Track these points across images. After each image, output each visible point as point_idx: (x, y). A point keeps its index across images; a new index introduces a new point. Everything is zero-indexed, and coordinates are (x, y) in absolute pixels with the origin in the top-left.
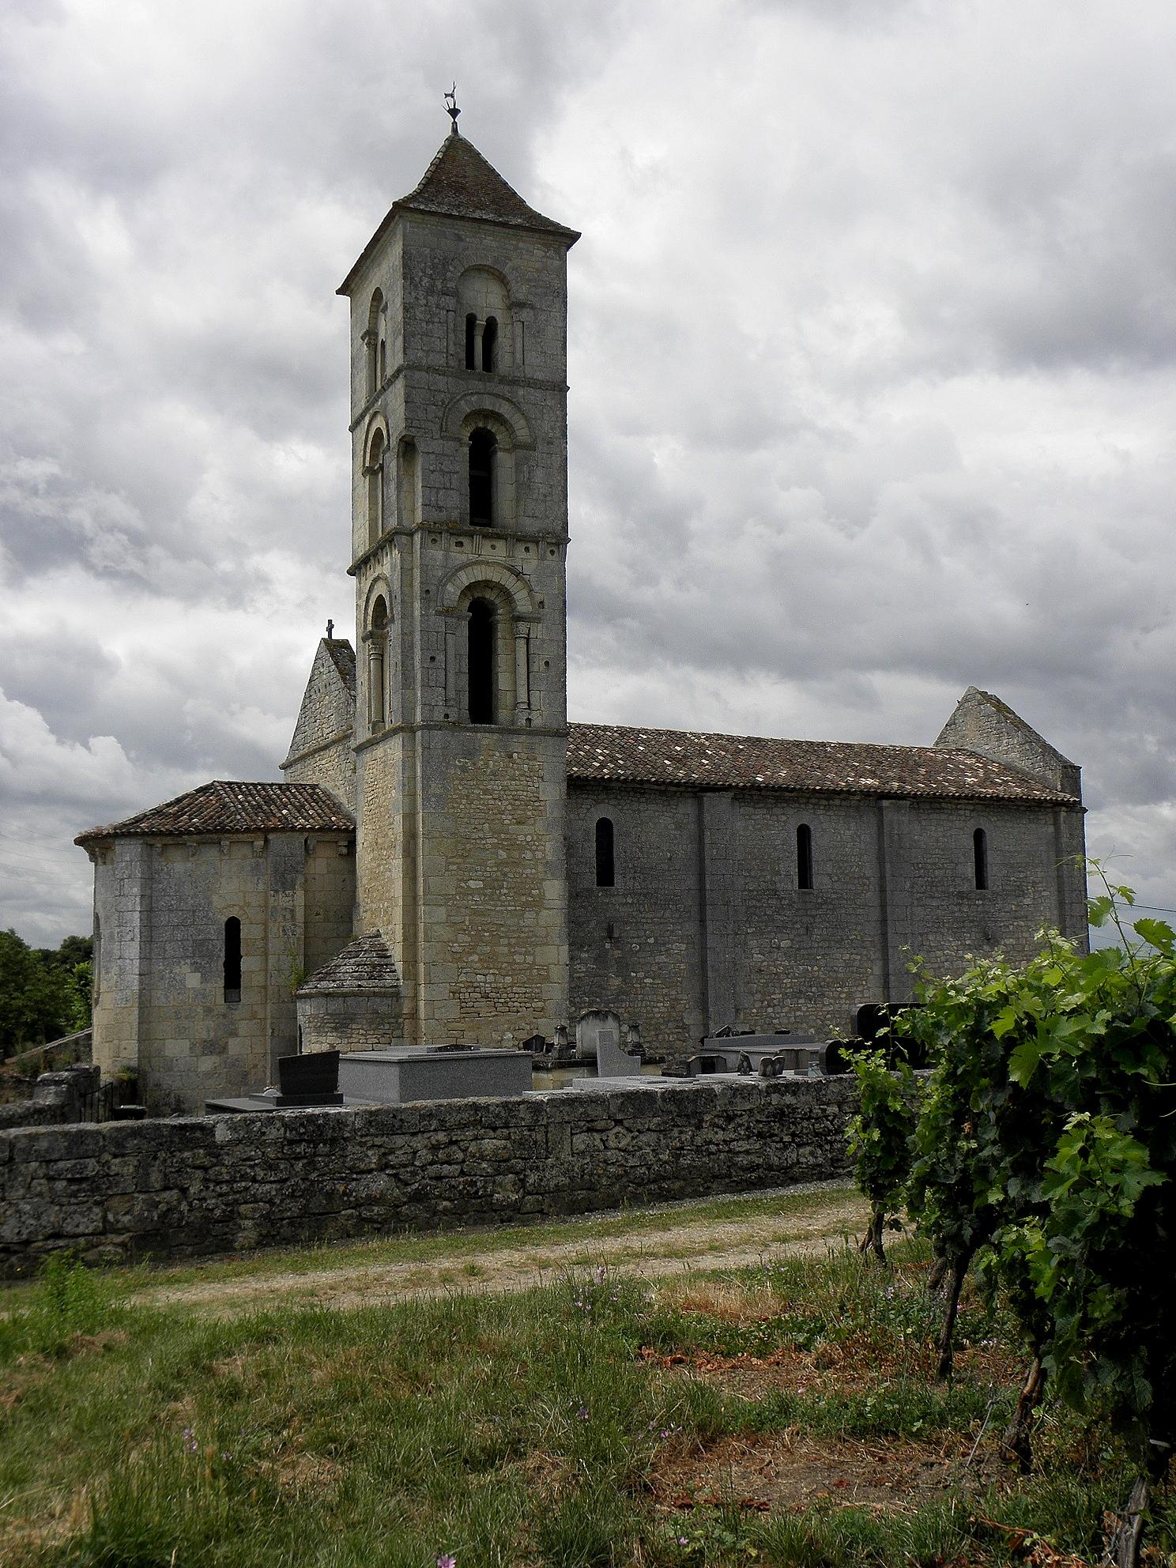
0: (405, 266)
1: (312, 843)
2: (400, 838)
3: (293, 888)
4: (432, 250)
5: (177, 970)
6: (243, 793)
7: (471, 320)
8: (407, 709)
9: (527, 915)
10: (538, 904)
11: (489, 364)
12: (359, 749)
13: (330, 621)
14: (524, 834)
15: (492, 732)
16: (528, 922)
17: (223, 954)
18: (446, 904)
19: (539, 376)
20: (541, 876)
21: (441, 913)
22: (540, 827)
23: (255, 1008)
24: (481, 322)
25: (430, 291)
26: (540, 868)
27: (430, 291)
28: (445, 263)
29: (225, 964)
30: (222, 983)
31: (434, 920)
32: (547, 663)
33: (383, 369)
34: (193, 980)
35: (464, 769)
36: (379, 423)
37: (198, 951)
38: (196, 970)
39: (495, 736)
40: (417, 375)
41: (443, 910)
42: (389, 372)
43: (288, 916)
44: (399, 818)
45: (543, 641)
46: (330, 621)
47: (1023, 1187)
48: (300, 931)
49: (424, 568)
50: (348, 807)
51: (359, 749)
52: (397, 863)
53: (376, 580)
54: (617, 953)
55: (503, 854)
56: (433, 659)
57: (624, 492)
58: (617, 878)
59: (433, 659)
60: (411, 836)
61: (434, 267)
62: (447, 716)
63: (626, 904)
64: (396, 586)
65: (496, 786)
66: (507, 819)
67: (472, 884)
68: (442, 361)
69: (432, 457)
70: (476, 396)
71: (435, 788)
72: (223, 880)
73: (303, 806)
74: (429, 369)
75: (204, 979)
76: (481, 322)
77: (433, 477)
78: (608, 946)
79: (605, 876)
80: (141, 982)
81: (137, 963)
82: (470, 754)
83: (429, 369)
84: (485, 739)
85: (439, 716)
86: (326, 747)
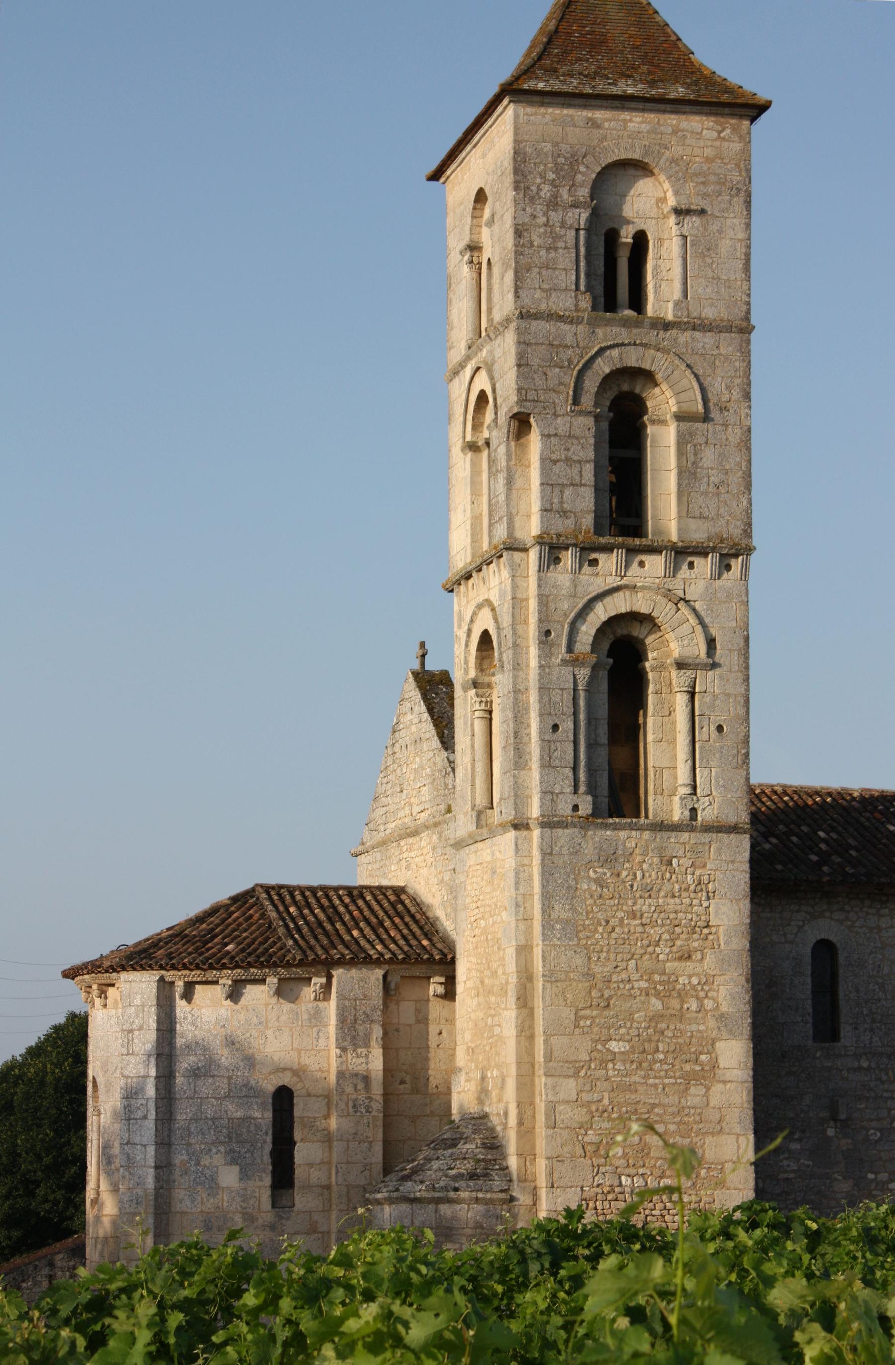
0: (516, 171)
1: (394, 979)
2: (513, 980)
3: (367, 1045)
4: (556, 144)
5: (206, 1161)
6: (296, 903)
7: (612, 236)
8: (519, 797)
9: (692, 1090)
10: (708, 1074)
11: (637, 301)
12: (459, 845)
13: (422, 645)
14: (686, 975)
15: (640, 828)
16: (696, 1101)
17: (269, 1139)
18: (576, 1075)
19: (709, 313)
20: (714, 1034)
21: (569, 1087)
22: (710, 962)
23: (316, 1217)
24: (627, 236)
25: (553, 203)
26: (711, 1023)
27: (553, 203)
28: (574, 160)
29: (273, 1153)
30: (268, 1180)
31: (561, 1096)
32: (720, 728)
33: (490, 310)
34: (229, 1177)
35: (600, 882)
36: (482, 382)
37: (234, 1141)
38: (233, 1161)
39: (647, 835)
40: (535, 325)
41: (571, 1083)
42: (497, 316)
43: (361, 1086)
44: (511, 952)
45: (715, 697)
46: (422, 645)
47: (239, 1317)
48: (377, 1105)
49: (544, 600)
50: (447, 924)
51: (459, 845)
52: (509, 1016)
53: (479, 607)
54: (845, 1143)
55: (656, 1004)
56: (555, 727)
57: (267, 1174)
58: (846, 1030)
59: (555, 727)
60: (526, 977)
61: (558, 169)
62: (576, 808)
63: (860, 1069)
64: (506, 621)
65: (645, 905)
66: (663, 951)
67: (614, 1046)
68: (570, 303)
69: (554, 441)
70: (617, 344)
71: (560, 911)
72: (270, 1033)
73: (381, 923)
74: (552, 316)
75: (244, 1175)
76: (627, 236)
77: (556, 469)
78: (831, 1132)
79: (827, 1028)
80: (157, 1178)
81: (151, 1150)
82: (610, 858)
83: (552, 316)
84: (626, 837)
85: (564, 809)
86: (415, 833)
